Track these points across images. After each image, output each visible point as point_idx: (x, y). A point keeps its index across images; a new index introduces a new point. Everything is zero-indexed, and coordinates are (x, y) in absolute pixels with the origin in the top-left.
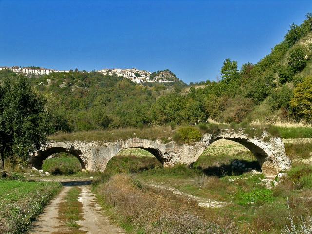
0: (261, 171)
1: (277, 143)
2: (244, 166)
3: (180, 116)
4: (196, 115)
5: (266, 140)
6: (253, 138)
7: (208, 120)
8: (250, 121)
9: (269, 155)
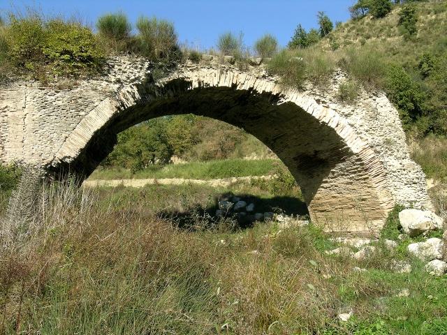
0: (308, 218)
1: (380, 110)
2: (250, 208)
3: (125, 152)
4: (151, 149)
5: (345, 97)
6: (301, 89)
7: (172, 159)
8: (241, 155)
9: (355, 151)
